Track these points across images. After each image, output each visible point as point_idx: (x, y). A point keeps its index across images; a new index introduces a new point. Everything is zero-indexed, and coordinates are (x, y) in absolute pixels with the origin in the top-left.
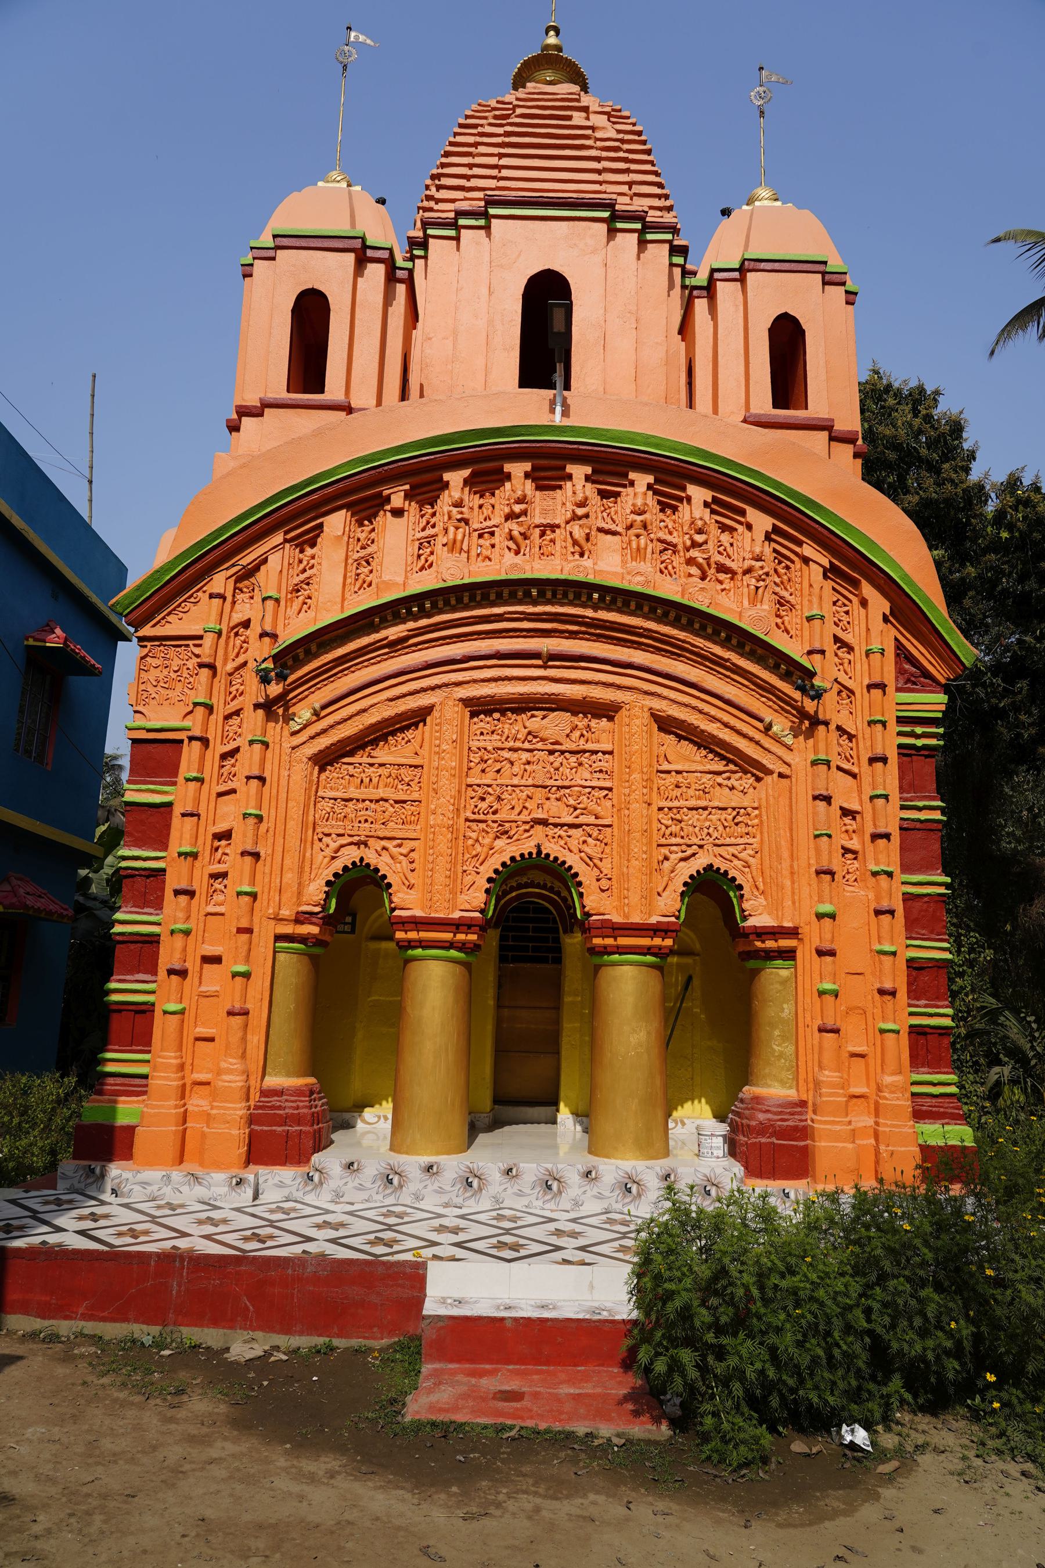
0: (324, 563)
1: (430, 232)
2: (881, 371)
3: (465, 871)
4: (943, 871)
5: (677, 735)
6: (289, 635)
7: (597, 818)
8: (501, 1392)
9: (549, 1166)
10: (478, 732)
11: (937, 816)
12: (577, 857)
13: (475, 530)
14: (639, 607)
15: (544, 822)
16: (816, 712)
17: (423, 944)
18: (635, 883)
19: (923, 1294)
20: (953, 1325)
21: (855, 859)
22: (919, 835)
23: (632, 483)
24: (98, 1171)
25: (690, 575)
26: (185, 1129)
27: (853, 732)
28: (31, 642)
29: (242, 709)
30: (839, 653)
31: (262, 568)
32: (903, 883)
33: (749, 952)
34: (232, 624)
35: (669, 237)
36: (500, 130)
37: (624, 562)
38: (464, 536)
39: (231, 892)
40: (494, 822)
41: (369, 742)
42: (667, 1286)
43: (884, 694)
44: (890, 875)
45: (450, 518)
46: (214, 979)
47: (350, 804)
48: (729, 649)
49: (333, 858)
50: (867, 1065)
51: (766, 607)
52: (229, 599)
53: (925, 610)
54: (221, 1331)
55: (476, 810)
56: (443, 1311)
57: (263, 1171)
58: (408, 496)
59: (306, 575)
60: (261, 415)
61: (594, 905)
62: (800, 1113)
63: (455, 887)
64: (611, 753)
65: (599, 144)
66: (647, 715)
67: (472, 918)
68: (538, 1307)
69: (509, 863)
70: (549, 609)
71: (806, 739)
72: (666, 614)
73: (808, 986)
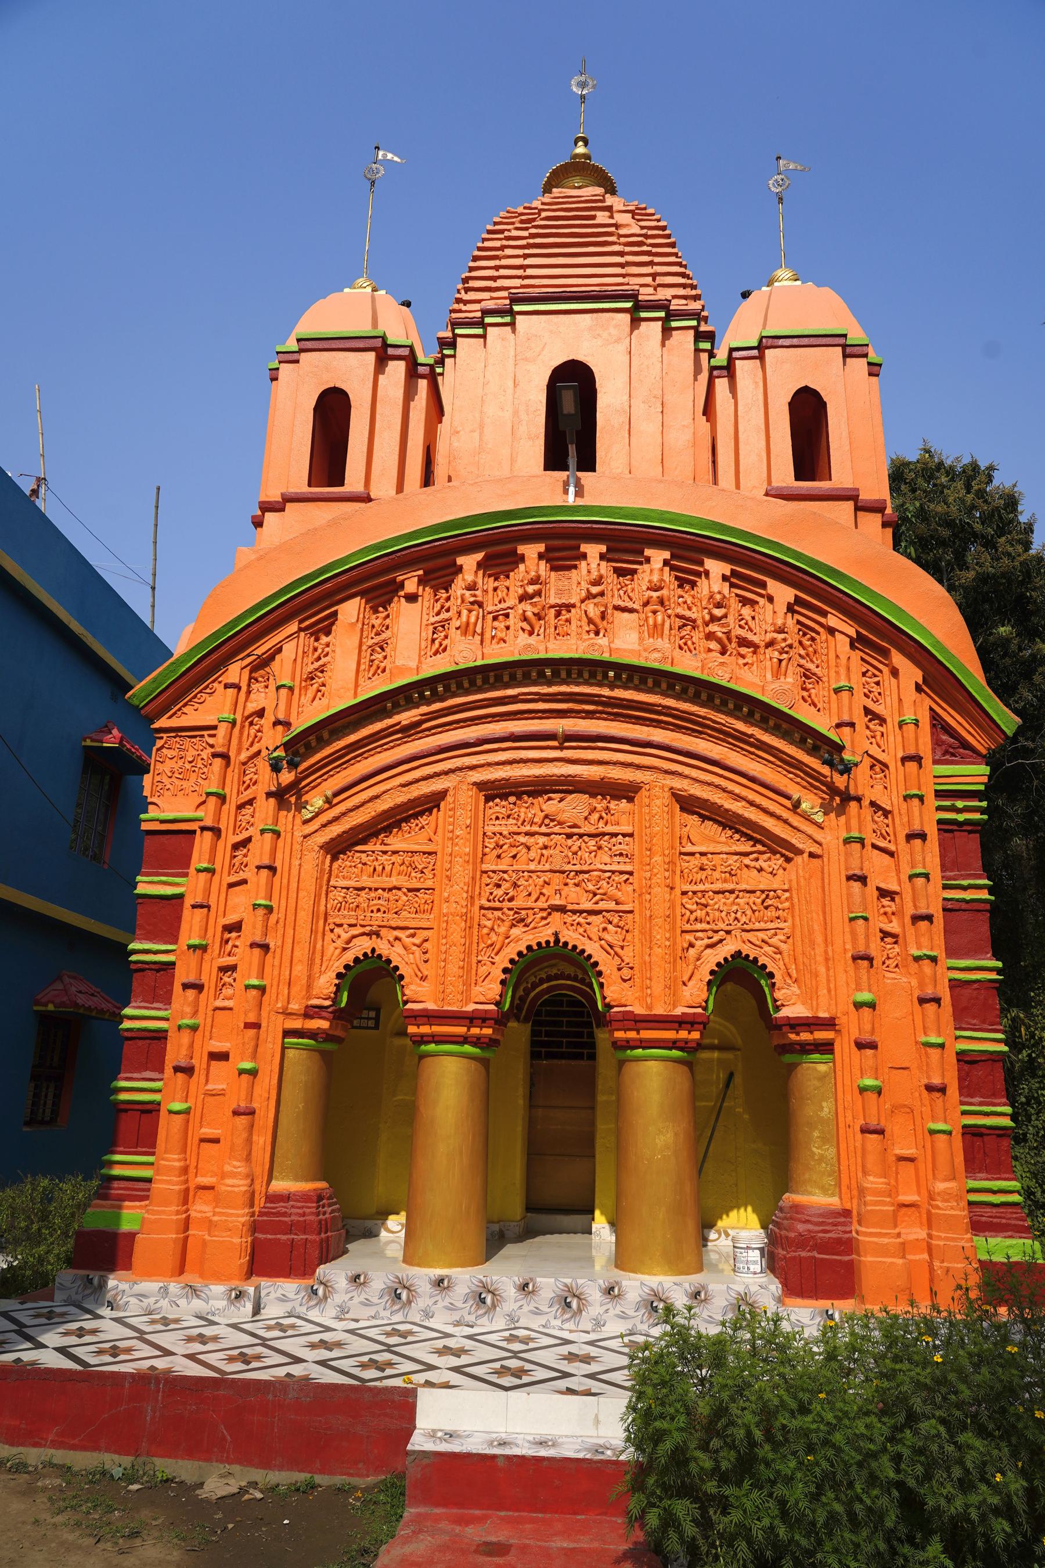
0: (338, 650)
1: (458, 331)
3: (480, 962)
4: (994, 955)
5: (701, 816)
6: (300, 725)
7: (617, 903)
8: (486, 1543)
9: (568, 1281)
10: (494, 817)
11: (984, 895)
12: (597, 945)
15: (562, 909)
16: (847, 787)
17: (436, 1039)
18: (658, 972)
19: (962, 1438)
20: (999, 1478)
21: (896, 943)
22: (966, 916)
23: (648, 560)
24: (96, 1281)
25: (710, 650)
26: (187, 1237)
27: (888, 808)
28: (88, 743)
29: (255, 798)
31: (277, 657)
32: (949, 969)
33: (784, 1045)
34: (246, 714)
35: (694, 323)
36: (525, 234)
37: (641, 639)
38: (478, 618)
39: (239, 986)
40: (510, 909)
42: (658, 1424)
43: (920, 767)
44: (934, 960)
45: (463, 601)
46: (221, 1078)
47: (363, 893)
48: (753, 725)
49: (345, 949)
52: (244, 688)
53: (960, 677)
55: (491, 898)
56: (429, 1446)
57: (265, 1283)
58: (421, 581)
59: (320, 663)
61: (615, 996)
62: (844, 1224)
63: (469, 978)
64: (631, 835)
65: (623, 240)
66: (667, 794)
67: (486, 1011)
69: (525, 952)
71: (838, 816)
72: (684, 691)
73: (848, 1082)
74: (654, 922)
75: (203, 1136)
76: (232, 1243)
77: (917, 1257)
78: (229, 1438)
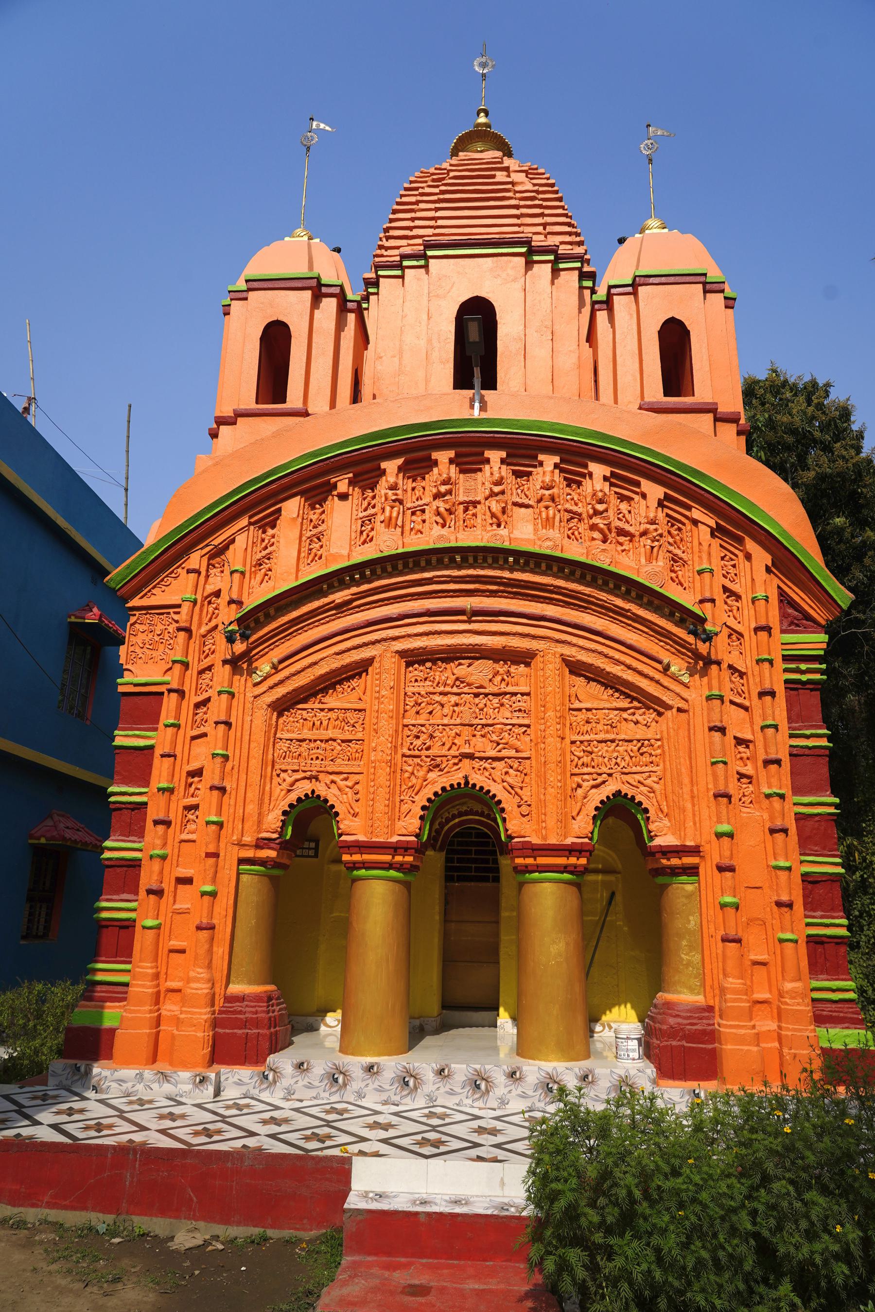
0: (281, 541)
1: (380, 273)
2: (779, 370)
3: (402, 801)
4: (832, 793)
5: (586, 677)
6: (250, 604)
7: (517, 751)
8: (410, 1286)
9: (478, 1067)
10: (413, 680)
11: (824, 743)
12: (500, 786)
13: (409, 509)
14: (549, 567)
15: (471, 756)
16: (709, 653)
17: (366, 865)
19: (807, 1196)
20: (839, 1229)
21: (750, 783)
22: (809, 760)
23: (541, 464)
24: (83, 1069)
25: (593, 539)
26: (159, 1032)
27: (743, 670)
28: (73, 619)
29: (213, 665)
30: (729, 601)
31: (231, 547)
32: (795, 804)
33: (658, 869)
34: (205, 594)
35: (578, 265)
36: (436, 190)
37: (536, 530)
38: (399, 513)
39: (201, 822)
41: (320, 690)
42: (554, 1186)
43: (770, 635)
44: (782, 797)
45: (386, 499)
46: (186, 898)
47: (304, 744)
48: (629, 601)
49: (289, 791)
50: (769, 973)
51: (661, 563)
52: (203, 573)
53: (803, 561)
54: (168, 1221)
55: (411, 747)
56: (363, 1205)
57: (224, 1070)
58: (351, 483)
59: (267, 551)
60: (235, 423)
61: (516, 829)
62: (708, 1018)
63: (393, 814)
64: (528, 694)
65: (518, 195)
66: (558, 660)
67: (408, 842)
68: (451, 1202)
69: (440, 792)
70: (471, 572)
71: (701, 677)
72: (572, 573)
73: (710, 900)
74: (547, 767)
76: (196, 1036)
77: (770, 1045)
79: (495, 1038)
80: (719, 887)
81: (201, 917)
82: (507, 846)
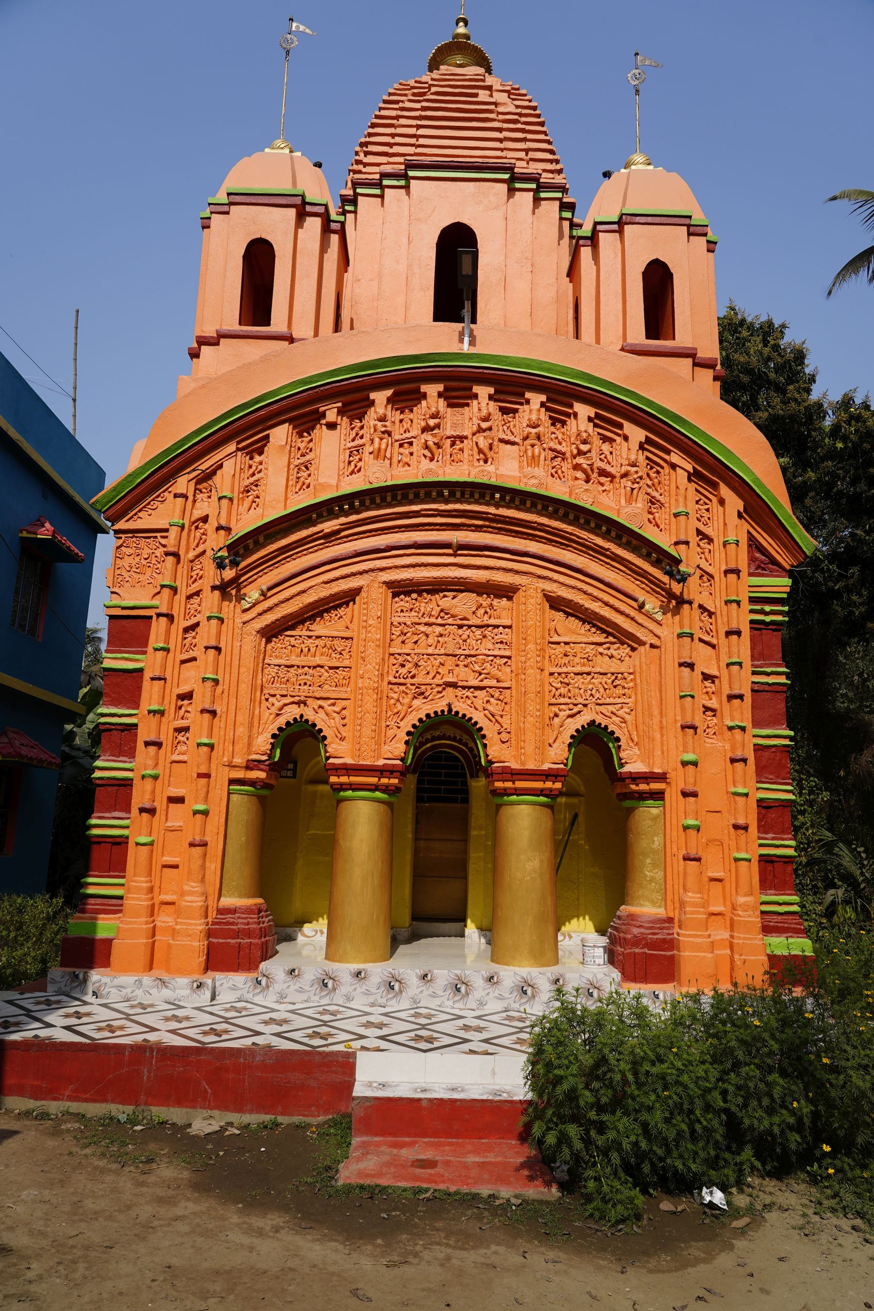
0: (269, 468)
1: (359, 191)
2: (737, 308)
4: (787, 726)
5: (565, 612)
7: (498, 681)
8: (418, 1160)
9: (458, 972)
10: (399, 610)
11: (783, 680)
14: (534, 505)
15: (454, 685)
16: (682, 593)
17: (353, 787)
18: (530, 736)
19: (770, 1078)
20: (795, 1104)
21: (714, 716)
23: (528, 402)
24: (81, 976)
25: (576, 479)
27: (712, 610)
28: (25, 534)
29: (201, 590)
31: (219, 472)
32: (754, 736)
33: (625, 794)
34: (193, 520)
35: (559, 195)
36: (418, 106)
37: (521, 468)
38: (387, 445)
39: (192, 743)
40: (412, 685)
41: (307, 618)
42: (557, 1072)
43: (739, 578)
44: (743, 729)
45: (375, 430)
46: (178, 816)
47: (292, 670)
48: (609, 541)
49: (278, 715)
51: (640, 505)
52: (191, 498)
53: (773, 508)
55: (397, 675)
56: (369, 1093)
57: (219, 976)
58: (340, 412)
59: (255, 478)
60: (218, 344)
61: (496, 754)
62: (668, 928)
64: (510, 627)
65: (501, 117)
66: (540, 595)
67: (394, 765)
68: (449, 1090)
69: (424, 719)
70: (458, 506)
71: (673, 615)
72: (556, 511)
73: (674, 822)
74: (527, 697)
75: (165, 863)
76: (192, 945)
77: (722, 952)
78: (209, 1091)
79: (463, 946)
80: (683, 811)
81: (194, 835)
82: (487, 770)
